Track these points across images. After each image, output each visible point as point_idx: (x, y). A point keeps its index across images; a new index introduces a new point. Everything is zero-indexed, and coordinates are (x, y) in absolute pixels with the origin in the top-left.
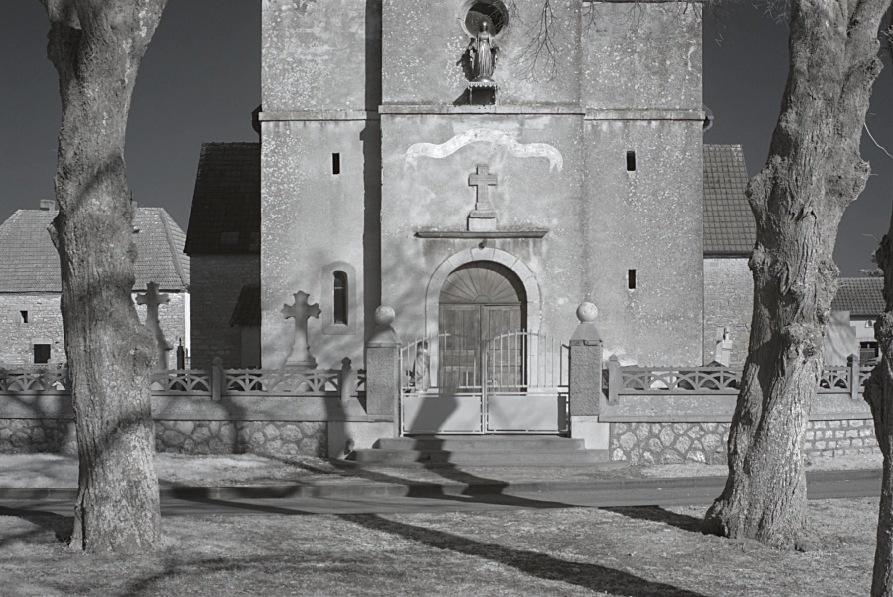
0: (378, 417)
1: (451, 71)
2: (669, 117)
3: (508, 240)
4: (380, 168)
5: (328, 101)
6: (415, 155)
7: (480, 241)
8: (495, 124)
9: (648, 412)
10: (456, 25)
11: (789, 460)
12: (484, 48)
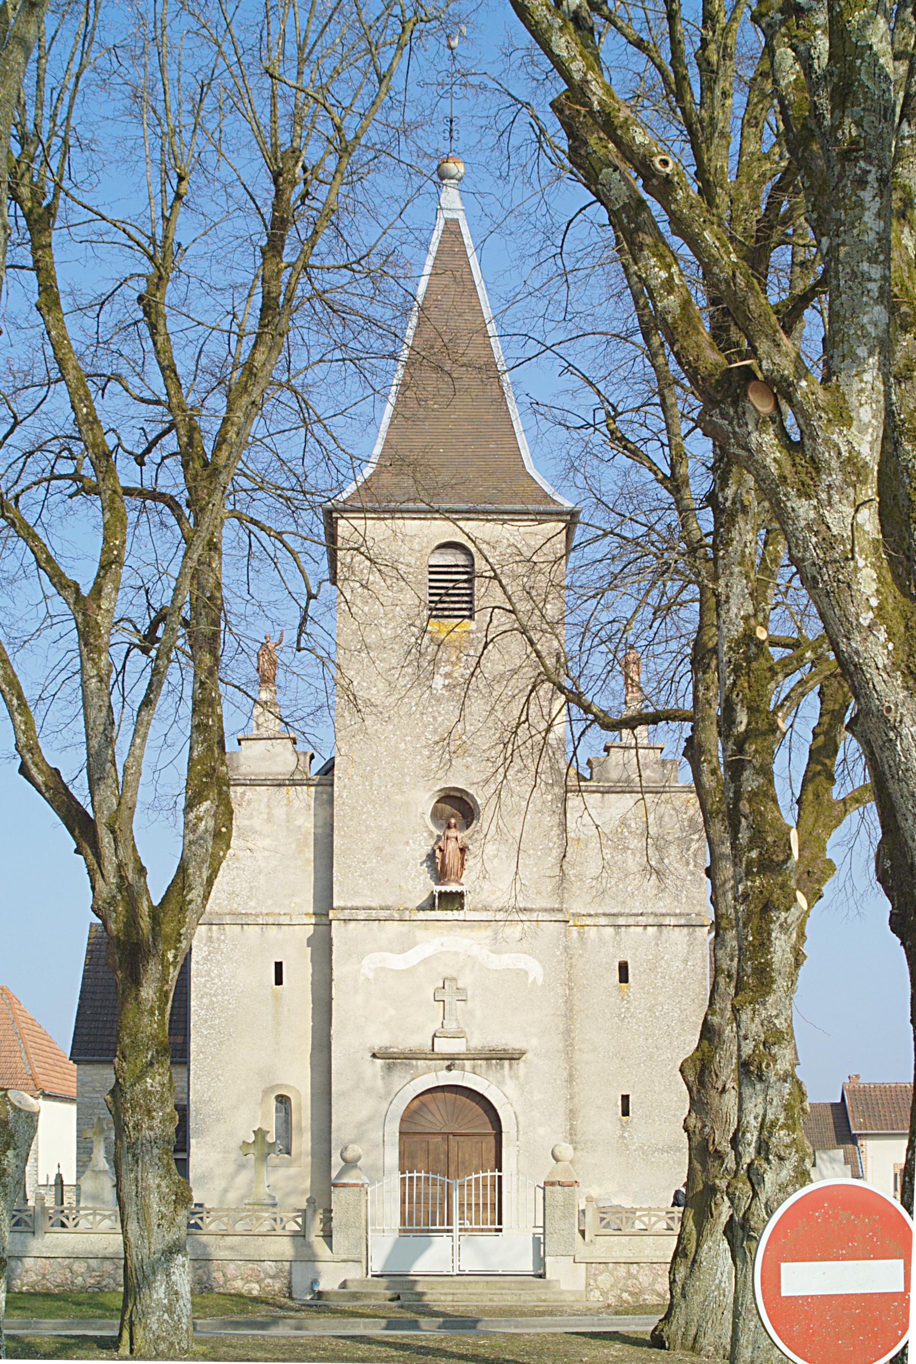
0: (344, 1257)
1: (413, 872)
2: (667, 923)
3: (480, 1062)
4: (332, 980)
5: (270, 902)
6: (372, 966)
7: (447, 1063)
8: (466, 932)
9: (626, 1253)
10: (420, 821)
11: (718, 1287)
12: (452, 847)
